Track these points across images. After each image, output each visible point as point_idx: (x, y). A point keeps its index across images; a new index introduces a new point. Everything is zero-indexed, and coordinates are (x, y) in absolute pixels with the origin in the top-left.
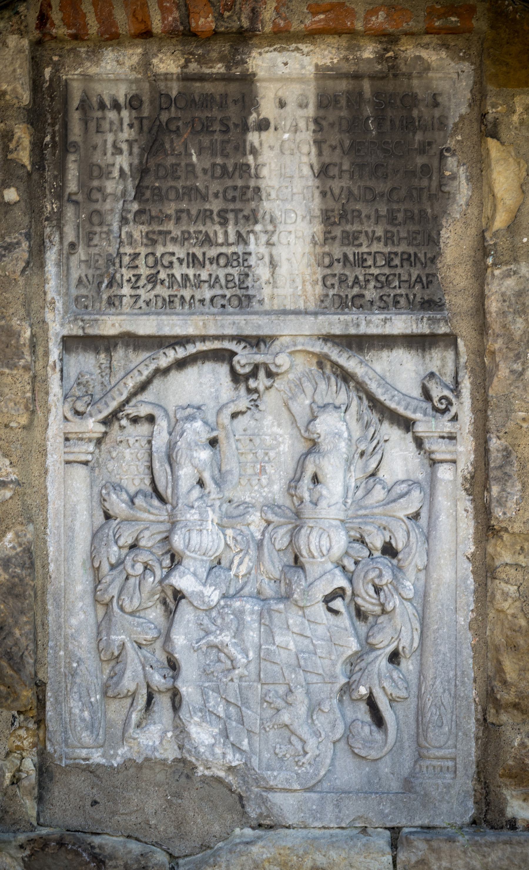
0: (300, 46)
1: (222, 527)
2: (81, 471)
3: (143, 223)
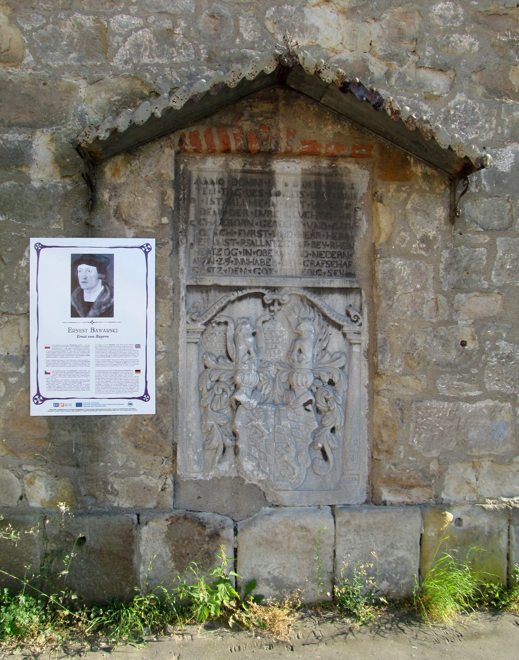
1: (258, 372)
2: (194, 347)
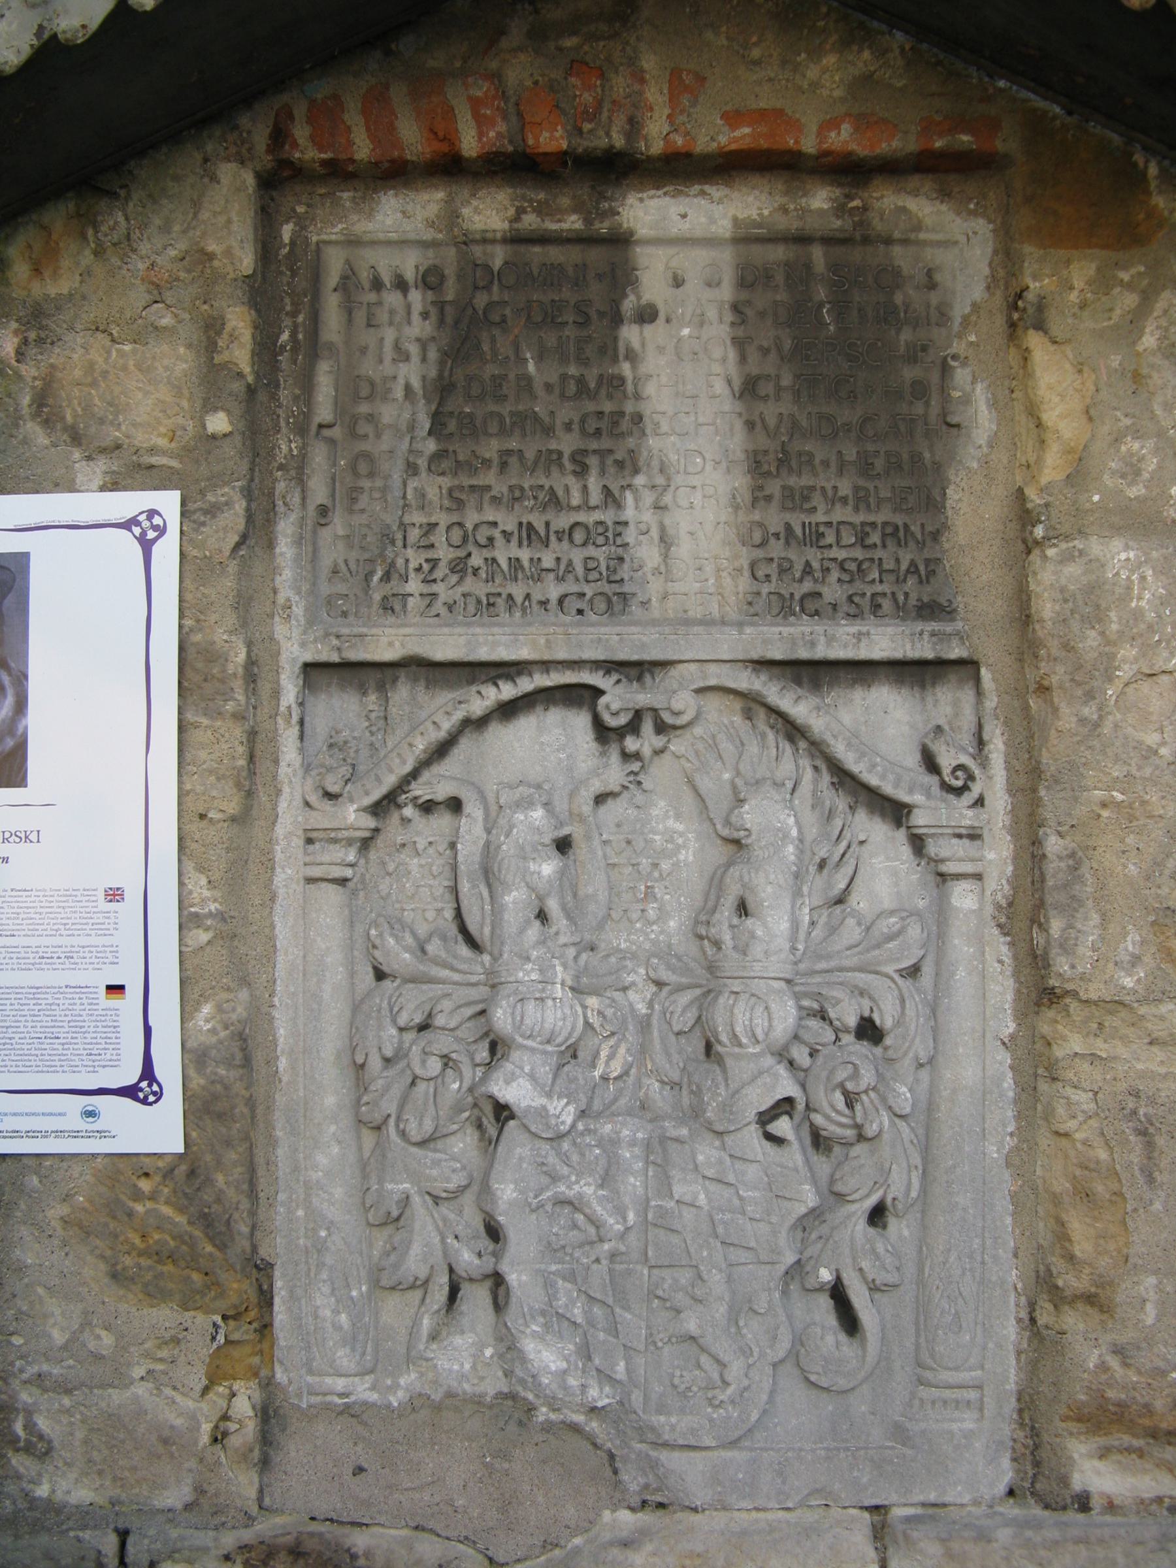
0: (707, 188)
3: (443, 474)
